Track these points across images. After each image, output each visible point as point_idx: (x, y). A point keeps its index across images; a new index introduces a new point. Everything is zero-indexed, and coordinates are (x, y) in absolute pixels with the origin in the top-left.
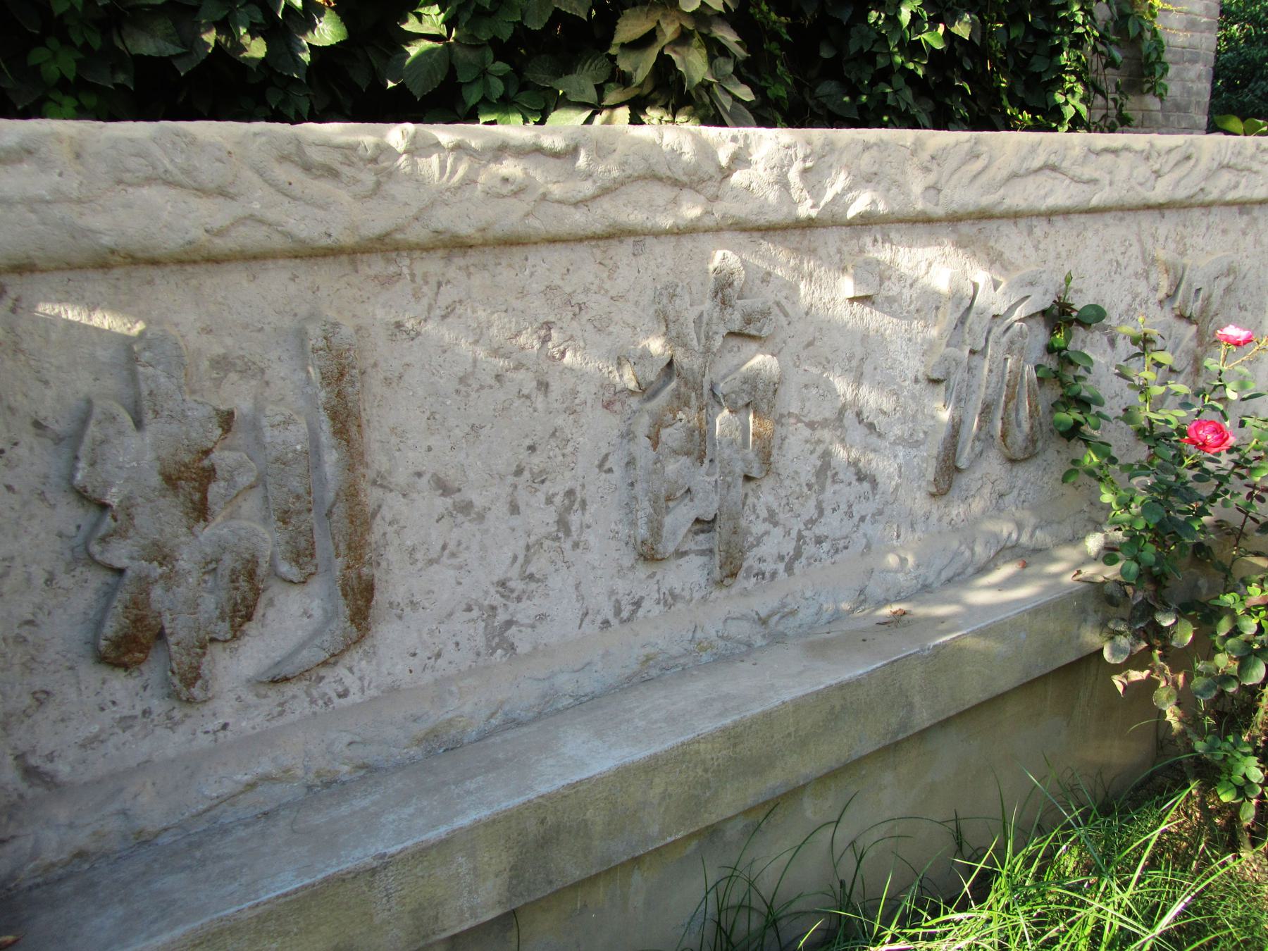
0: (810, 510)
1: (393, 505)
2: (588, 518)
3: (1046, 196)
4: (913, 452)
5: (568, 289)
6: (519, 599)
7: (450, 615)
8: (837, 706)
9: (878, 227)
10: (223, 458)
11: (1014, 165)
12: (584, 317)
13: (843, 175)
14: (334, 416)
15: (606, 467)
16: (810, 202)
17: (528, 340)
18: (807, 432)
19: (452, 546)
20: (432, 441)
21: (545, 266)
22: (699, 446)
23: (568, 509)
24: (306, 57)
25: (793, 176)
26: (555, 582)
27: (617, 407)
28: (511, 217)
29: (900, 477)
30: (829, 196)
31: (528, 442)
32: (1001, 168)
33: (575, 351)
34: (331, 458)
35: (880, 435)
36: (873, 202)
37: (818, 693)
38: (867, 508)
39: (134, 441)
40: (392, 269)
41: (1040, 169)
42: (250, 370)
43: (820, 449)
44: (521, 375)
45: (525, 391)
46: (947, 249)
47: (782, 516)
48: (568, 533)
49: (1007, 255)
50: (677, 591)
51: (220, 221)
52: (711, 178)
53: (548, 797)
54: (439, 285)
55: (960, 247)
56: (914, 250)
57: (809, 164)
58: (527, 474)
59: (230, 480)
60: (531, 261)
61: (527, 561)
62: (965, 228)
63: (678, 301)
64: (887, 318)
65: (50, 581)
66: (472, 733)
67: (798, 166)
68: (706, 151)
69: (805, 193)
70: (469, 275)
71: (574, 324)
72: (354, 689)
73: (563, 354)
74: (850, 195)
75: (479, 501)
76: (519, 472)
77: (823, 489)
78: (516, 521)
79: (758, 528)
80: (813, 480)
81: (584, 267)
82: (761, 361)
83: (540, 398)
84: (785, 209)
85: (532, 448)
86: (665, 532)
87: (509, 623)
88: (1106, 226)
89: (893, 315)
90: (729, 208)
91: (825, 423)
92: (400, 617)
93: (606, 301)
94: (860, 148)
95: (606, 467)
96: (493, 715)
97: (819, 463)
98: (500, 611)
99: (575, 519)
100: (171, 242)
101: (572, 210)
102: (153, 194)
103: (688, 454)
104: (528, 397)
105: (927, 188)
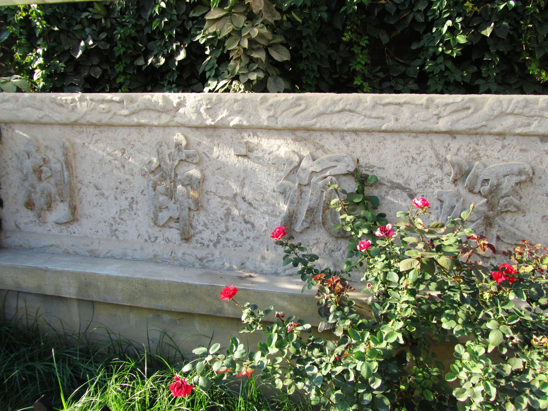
0: (222, 227)
1: (84, 189)
2: (138, 207)
3: (346, 123)
4: (274, 219)
5: (129, 140)
6: (119, 224)
7: (100, 222)
8: (188, 291)
9: (251, 130)
10: (44, 168)
11: (322, 109)
12: (134, 148)
13: (226, 111)
14: (66, 163)
15: (144, 193)
16: (211, 120)
17: (118, 153)
18: (220, 200)
19: (100, 203)
20: (94, 175)
21: (122, 133)
22: (171, 194)
23: (132, 203)
24: (177, 63)
25: (202, 110)
26: (129, 222)
27: (146, 176)
28: (106, 119)
29: (267, 227)
30: (219, 118)
31: (119, 181)
32: (313, 110)
33: (132, 158)
34: (66, 173)
35: (255, 208)
36: (240, 121)
37: (178, 283)
38: (252, 234)
39: (28, 161)
40: (82, 130)
41: (340, 112)
42: (51, 149)
43: (226, 207)
44: (116, 162)
45: (118, 167)
46: (289, 142)
47: (210, 226)
48: (132, 210)
49: (326, 146)
50: (170, 238)
51: (41, 116)
52: (171, 110)
53: (88, 273)
54: (93, 135)
55: (297, 141)
56: (270, 140)
57: (209, 107)
58: (119, 190)
59: (46, 173)
60: (117, 131)
61: (120, 214)
62: (300, 134)
63: (163, 148)
64: (256, 165)
65: (18, 187)
66: (102, 255)
67: (204, 107)
68: (167, 101)
69: (208, 116)
70: (101, 133)
71: (132, 150)
72: (77, 232)
73: (129, 158)
74: (230, 118)
75: (107, 194)
76: (117, 188)
77: (227, 221)
78: (116, 202)
79: (200, 228)
80: (223, 217)
81: (134, 134)
82: (195, 172)
83: (122, 169)
84: (200, 122)
85: (120, 183)
86: (159, 217)
87: (116, 230)
88: (402, 139)
89: (260, 164)
90: (178, 119)
91: (227, 198)
92: (87, 218)
93: (141, 145)
94: (233, 101)
95: (144, 193)
96: (108, 253)
97: (225, 212)
98: (114, 225)
99: (134, 206)
100: (32, 120)
101: (124, 118)
102: (29, 109)
103: (166, 195)
104: (119, 168)
105: (269, 117)
